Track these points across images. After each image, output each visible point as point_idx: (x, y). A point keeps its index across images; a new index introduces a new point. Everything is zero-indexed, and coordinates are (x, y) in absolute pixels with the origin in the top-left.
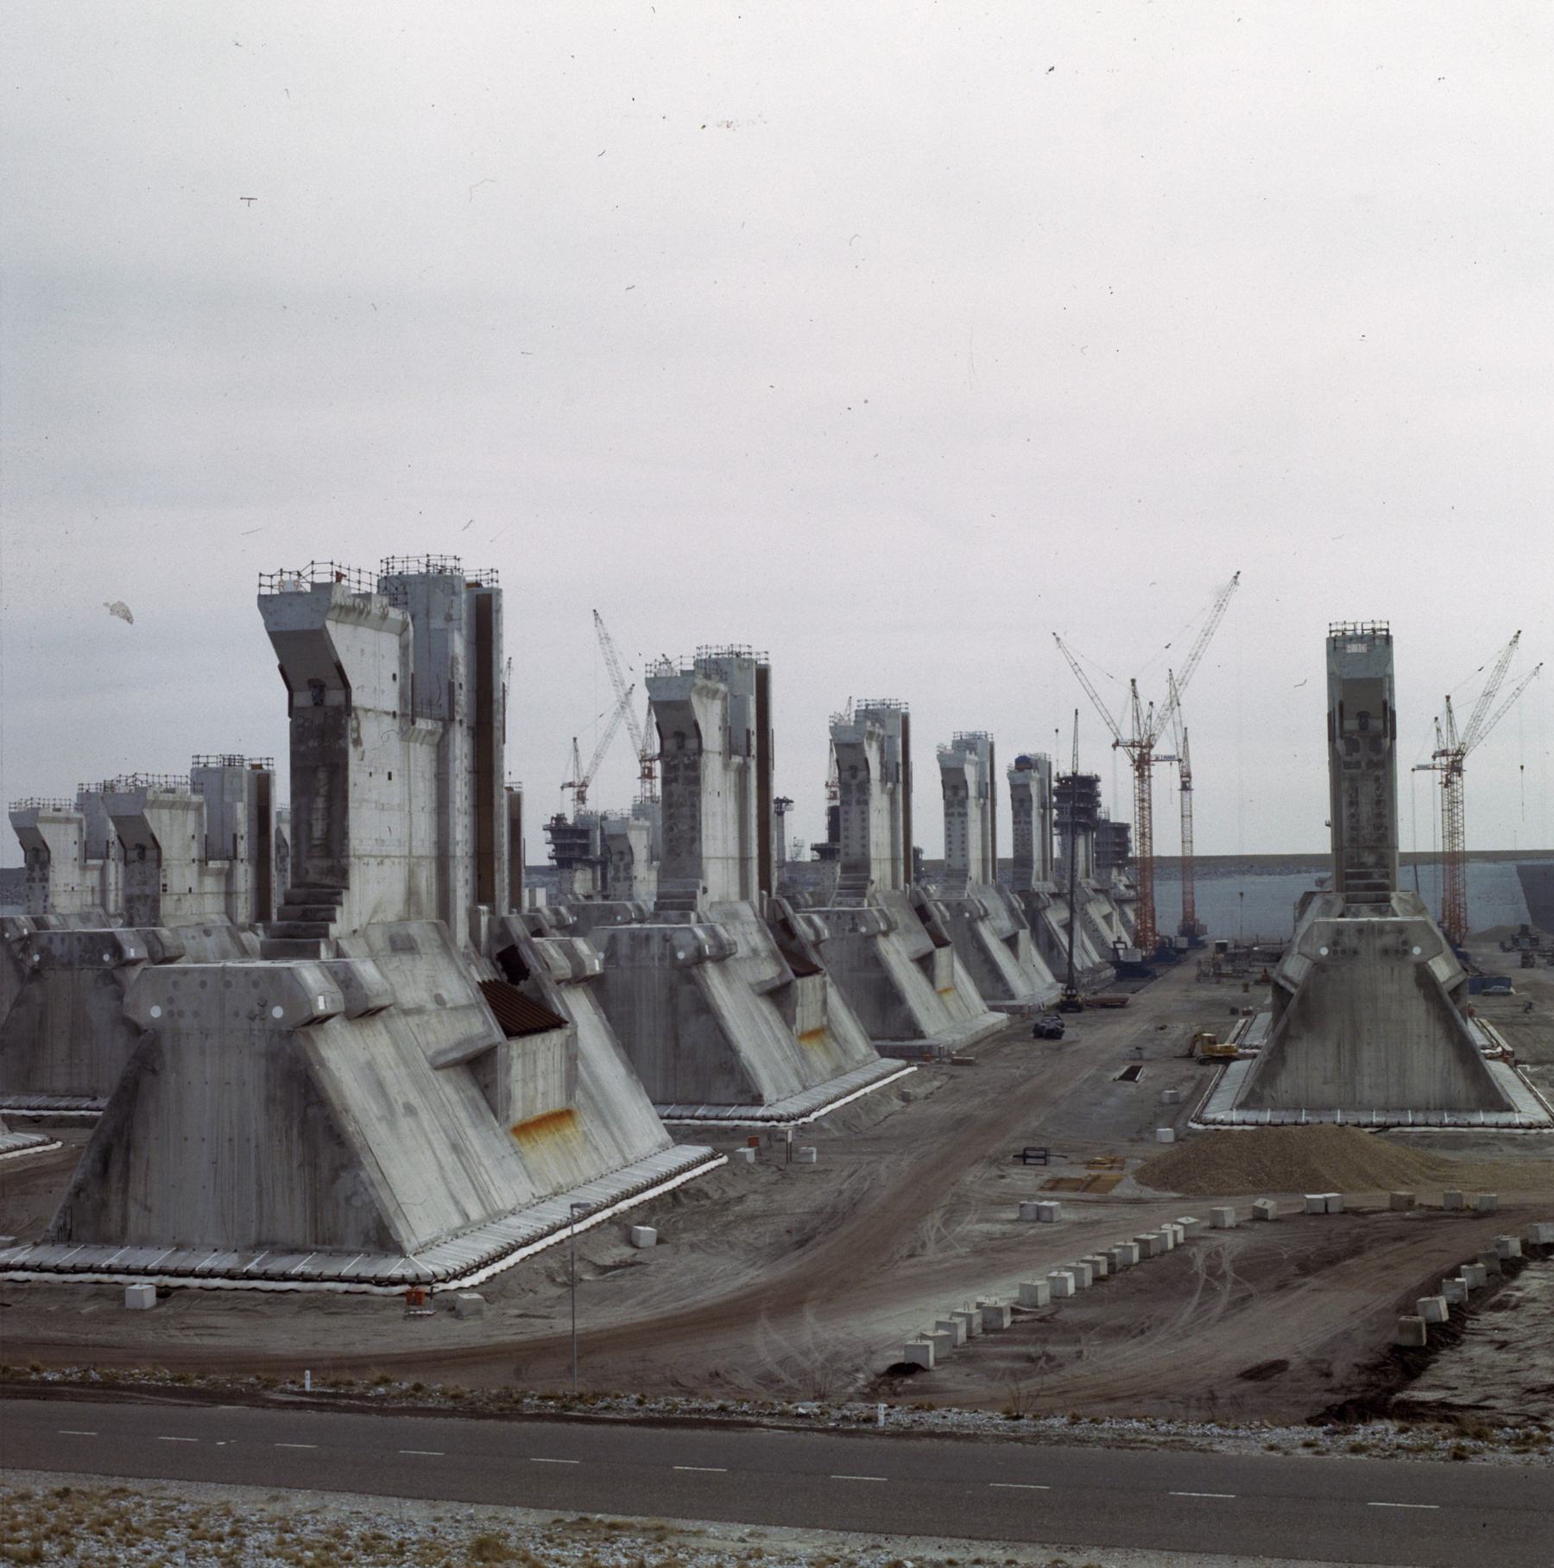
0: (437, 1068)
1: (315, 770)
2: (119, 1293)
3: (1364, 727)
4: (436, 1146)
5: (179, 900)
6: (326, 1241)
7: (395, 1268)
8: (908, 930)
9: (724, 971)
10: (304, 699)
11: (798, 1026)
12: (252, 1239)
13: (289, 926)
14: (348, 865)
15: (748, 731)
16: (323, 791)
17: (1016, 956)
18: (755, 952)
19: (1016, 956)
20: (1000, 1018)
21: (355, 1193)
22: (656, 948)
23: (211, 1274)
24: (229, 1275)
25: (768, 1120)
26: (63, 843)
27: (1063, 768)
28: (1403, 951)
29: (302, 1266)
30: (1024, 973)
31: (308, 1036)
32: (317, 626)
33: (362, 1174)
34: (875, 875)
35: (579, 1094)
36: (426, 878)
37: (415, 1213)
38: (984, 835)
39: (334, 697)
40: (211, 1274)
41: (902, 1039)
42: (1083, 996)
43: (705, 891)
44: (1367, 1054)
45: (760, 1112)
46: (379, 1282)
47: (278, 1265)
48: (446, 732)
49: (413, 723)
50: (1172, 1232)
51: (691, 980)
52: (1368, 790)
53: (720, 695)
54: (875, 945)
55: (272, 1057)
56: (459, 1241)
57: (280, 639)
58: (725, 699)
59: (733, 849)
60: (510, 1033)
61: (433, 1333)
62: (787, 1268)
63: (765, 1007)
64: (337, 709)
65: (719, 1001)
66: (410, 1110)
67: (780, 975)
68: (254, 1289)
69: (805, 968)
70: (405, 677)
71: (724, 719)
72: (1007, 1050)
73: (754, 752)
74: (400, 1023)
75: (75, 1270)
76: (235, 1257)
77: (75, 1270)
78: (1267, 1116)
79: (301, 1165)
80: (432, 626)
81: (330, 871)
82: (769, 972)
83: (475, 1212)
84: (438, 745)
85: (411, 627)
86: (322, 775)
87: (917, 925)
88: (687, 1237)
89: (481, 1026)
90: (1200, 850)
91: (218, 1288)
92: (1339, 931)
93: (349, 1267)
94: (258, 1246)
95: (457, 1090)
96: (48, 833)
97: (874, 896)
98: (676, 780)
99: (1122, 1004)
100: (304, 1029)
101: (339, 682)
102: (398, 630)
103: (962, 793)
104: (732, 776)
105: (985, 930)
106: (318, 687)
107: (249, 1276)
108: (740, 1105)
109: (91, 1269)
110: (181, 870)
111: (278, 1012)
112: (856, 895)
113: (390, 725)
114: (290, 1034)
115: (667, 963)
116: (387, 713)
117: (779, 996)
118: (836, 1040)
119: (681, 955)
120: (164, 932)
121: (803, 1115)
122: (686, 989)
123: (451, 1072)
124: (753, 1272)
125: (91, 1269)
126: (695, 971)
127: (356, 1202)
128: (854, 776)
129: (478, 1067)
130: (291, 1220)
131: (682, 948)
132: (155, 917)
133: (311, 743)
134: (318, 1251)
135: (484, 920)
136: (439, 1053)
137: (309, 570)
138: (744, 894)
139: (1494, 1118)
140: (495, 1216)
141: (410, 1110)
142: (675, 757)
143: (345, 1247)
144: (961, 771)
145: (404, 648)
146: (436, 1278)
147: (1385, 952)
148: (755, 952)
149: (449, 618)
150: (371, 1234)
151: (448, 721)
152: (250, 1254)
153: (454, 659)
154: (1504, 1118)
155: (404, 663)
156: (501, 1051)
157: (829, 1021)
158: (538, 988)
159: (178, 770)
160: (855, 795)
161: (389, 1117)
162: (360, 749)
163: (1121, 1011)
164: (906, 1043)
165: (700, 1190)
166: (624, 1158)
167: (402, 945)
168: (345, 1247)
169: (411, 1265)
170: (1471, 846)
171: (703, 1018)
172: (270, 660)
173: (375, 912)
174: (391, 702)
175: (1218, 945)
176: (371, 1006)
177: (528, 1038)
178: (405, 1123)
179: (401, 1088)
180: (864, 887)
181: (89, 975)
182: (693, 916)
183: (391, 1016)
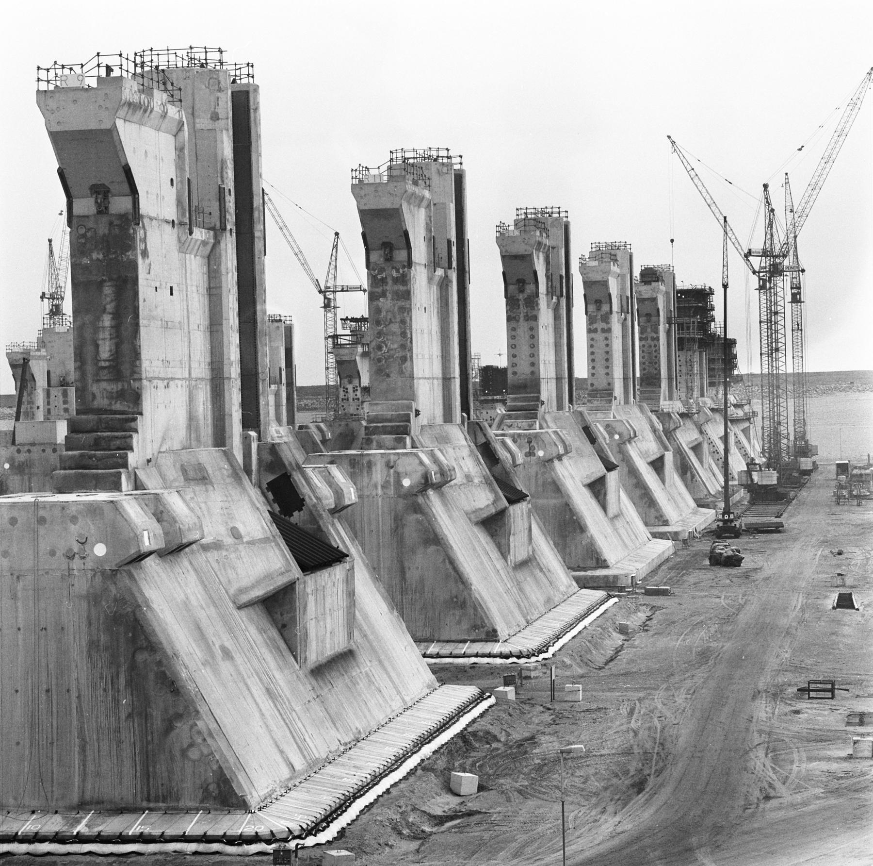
0: (240, 608)
1: (101, 284)
4: (254, 691)
5: (732, 421)
6: (160, 797)
7: (244, 825)
8: (580, 454)
9: (442, 496)
10: (86, 206)
11: (511, 558)
12: (75, 799)
13: (82, 456)
14: (140, 388)
15: (449, 242)
16: (110, 307)
17: (663, 481)
18: (468, 478)
19: (663, 481)
20: (665, 546)
21: (191, 745)
25: (507, 657)
27: (686, 280)
30: (671, 498)
31: (131, 576)
32: (106, 125)
33: (200, 724)
34: (544, 396)
35: (356, 633)
36: (203, 396)
38: (624, 351)
39: (120, 204)
41: (585, 569)
42: (740, 523)
43: (417, 413)
45: (497, 648)
46: (231, 841)
47: (112, 825)
48: (217, 242)
49: (191, 233)
51: (417, 509)
53: (425, 203)
54: (553, 469)
56: (292, 794)
57: (62, 140)
58: (428, 206)
59: (437, 370)
63: (482, 537)
64: (123, 217)
65: (446, 532)
66: (227, 654)
67: (495, 502)
68: (90, 853)
69: (515, 497)
70: (182, 182)
71: (428, 229)
72: (691, 579)
73: (454, 264)
74: (201, 558)
76: (58, 818)
79: (130, 716)
80: (198, 126)
81: (120, 395)
83: (299, 764)
84: (209, 257)
85: (186, 128)
86: (108, 290)
87: (588, 448)
88: (506, 782)
89: (273, 563)
91: (49, 854)
93: (192, 825)
94: (82, 806)
95: (261, 631)
97: (544, 418)
98: (384, 294)
99: (777, 529)
100: (126, 568)
101: (126, 188)
102: (175, 130)
103: (605, 308)
104: (435, 288)
105: (633, 451)
106: (101, 192)
107: (80, 839)
108: (473, 641)
112: (526, 418)
113: (170, 235)
114: (114, 573)
115: (391, 491)
116: (167, 222)
117: (493, 524)
118: (541, 570)
119: (406, 483)
121: (540, 652)
123: (250, 610)
126: (420, 500)
127: (194, 754)
128: (521, 291)
129: (278, 608)
130: (119, 777)
131: (406, 475)
133: (95, 256)
134: (151, 810)
135: (254, 446)
136: (242, 591)
137: (95, 62)
138: (448, 417)
140: (316, 766)
141: (227, 654)
142: (382, 270)
143: (181, 804)
144: (605, 284)
145: (180, 150)
146: (291, 835)
148: (468, 478)
149: (215, 117)
150: (212, 787)
151: (218, 231)
152: (73, 814)
153: (223, 162)
155: (180, 168)
156: (299, 587)
157: (534, 551)
158: (314, 518)
160: (523, 310)
161: (210, 662)
162: (147, 261)
163: (775, 536)
164: (589, 573)
165: (488, 733)
166: (403, 700)
167: (197, 476)
168: (181, 804)
169: (260, 820)
171: (432, 549)
173: (164, 439)
174: (170, 212)
175: (838, 465)
176: (185, 541)
177: (319, 573)
178: (225, 667)
179: (219, 637)
180: (535, 408)
182: (408, 441)
183: (193, 552)
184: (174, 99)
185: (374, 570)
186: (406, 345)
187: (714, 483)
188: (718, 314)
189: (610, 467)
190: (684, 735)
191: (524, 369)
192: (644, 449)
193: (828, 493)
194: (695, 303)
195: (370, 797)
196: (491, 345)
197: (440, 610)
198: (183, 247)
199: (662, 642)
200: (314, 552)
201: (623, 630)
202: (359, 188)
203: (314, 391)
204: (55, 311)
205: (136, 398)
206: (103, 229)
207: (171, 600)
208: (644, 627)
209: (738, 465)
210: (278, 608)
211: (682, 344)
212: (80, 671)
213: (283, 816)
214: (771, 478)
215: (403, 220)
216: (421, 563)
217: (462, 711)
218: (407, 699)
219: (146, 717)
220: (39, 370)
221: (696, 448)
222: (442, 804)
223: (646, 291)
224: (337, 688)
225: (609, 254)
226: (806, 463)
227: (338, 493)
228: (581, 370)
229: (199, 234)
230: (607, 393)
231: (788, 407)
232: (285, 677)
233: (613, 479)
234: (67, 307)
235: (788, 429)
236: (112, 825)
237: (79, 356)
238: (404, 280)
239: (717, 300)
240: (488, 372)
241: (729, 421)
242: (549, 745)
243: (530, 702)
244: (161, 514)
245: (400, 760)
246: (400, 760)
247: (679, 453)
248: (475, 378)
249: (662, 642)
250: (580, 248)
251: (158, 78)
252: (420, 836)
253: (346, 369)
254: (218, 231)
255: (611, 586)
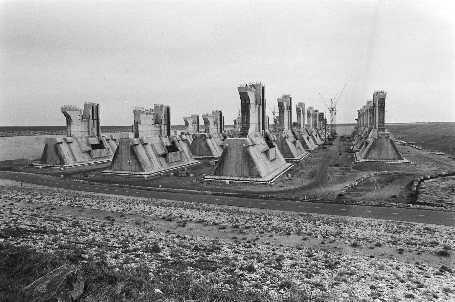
2: (225, 182)
3: (381, 105)
6: (251, 176)
7: (261, 180)
10: (243, 102)
20: (317, 146)
22: (279, 136)
23: (236, 180)
24: (238, 180)
26: (190, 122)
27: (320, 112)
28: (388, 137)
29: (248, 179)
36: (257, 126)
37: (263, 172)
40: (236, 180)
44: (382, 152)
46: (260, 181)
47: (245, 179)
50: (366, 176)
51: (285, 141)
52: (382, 114)
55: (243, 151)
57: (240, 94)
60: (270, 148)
61: (269, 189)
62: (313, 181)
69: (297, 139)
75: (217, 179)
77: (217, 179)
78: (367, 160)
82: (293, 139)
83: (268, 172)
89: (266, 147)
90: (334, 123)
92: (379, 134)
93: (255, 179)
94: (242, 176)
96: (188, 121)
99: (332, 144)
105: (313, 134)
106: (245, 100)
107: (241, 180)
109: (219, 179)
110: (212, 126)
111: (244, 145)
113: (254, 105)
117: (294, 143)
120: (210, 134)
122: (284, 142)
124: (308, 182)
125: (219, 179)
129: (266, 152)
130: (246, 173)
132: (209, 132)
138: (289, 129)
139: (401, 161)
140: (270, 173)
147: (386, 137)
151: (260, 105)
154: (403, 161)
158: (271, 141)
159: (210, 112)
161: (258, 159)
167: (256, 136)
170: (338, 122)
172: (239, 96)
174: (254, 103)
178: (259, 160)
179: (259, 155)
181: (201, 139)
184: (255, 88)
185: (279, 148)
186: (283, 120)
187: (323, 138)
188: (325, 116)
189: (310, 136)
190: (318, 170)
191: (299, 123)
192: (314, 133)
193: (338, 140)
194: (322, 115)
195: (277, 177)
196: (294, 120)
197: (287, 153)
198: (255, 107)
199: (316, 158)
200: (271, 146)
201: (311, 157)
202: (278, 99)
203: (272, 125)
204: (239, 115)
205: (249, 126)
206: (245, 105)
207: (253, 151)
208: (314, 156)
209: (327, 136)
210: (266, 152)
211: (320, 120)
212: (241, 159)
213: (267, 179)
214: (331, 138)
215: (283, 105)
216: (285, 147)
217: (289, 167)
218: (283, 164)
219: (249, 166)
220: (237, 122)
221: (321, 133)
222: (287, 178)
223: (315, 113)
224: (274, 163)
225: (310, 108)
226: (336, 136)
227: (274, 138)
228: (306, 123)
229: (258, 105)
230: (310, 126)
231: (334, 128)
232: (268, 162)
233: (310, 137)
234: (241, 114)
235: (334, 131)
236: (245, 179)
237: (242, 120)
238: (283, 111)
239: (325, 114)
240: (294, 123)
241: (326, 130)
242: (301, 171)
243: (298, 166)
244: (252, 141)
245: (281, 172)
246: (281, 172)
247: (319, 134)
248: (292, 124)
249: (316, 158)
250: (307, 107)
251: (253, 86)
252: (284, 182)
253: (276, 122)
254: (260, 105)
255: (309, 151)
